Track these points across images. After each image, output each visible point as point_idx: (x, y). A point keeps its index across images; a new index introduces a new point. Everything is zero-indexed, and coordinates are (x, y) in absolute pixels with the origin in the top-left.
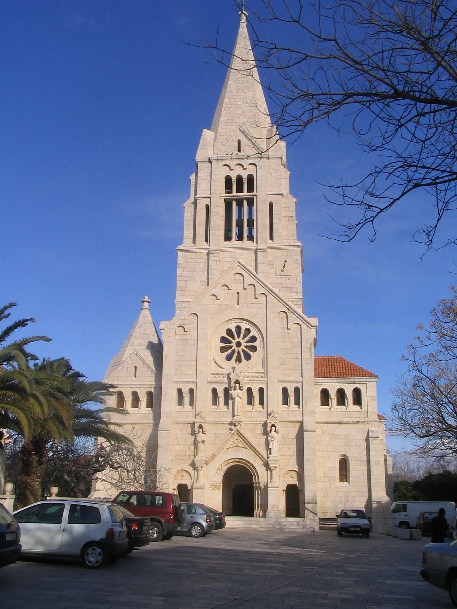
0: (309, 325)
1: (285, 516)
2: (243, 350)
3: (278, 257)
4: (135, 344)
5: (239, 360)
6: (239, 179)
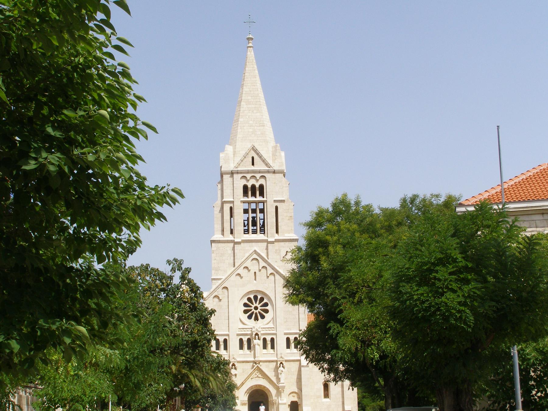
2: (259, 312)
5: (256, 319)
6: (253, 187)
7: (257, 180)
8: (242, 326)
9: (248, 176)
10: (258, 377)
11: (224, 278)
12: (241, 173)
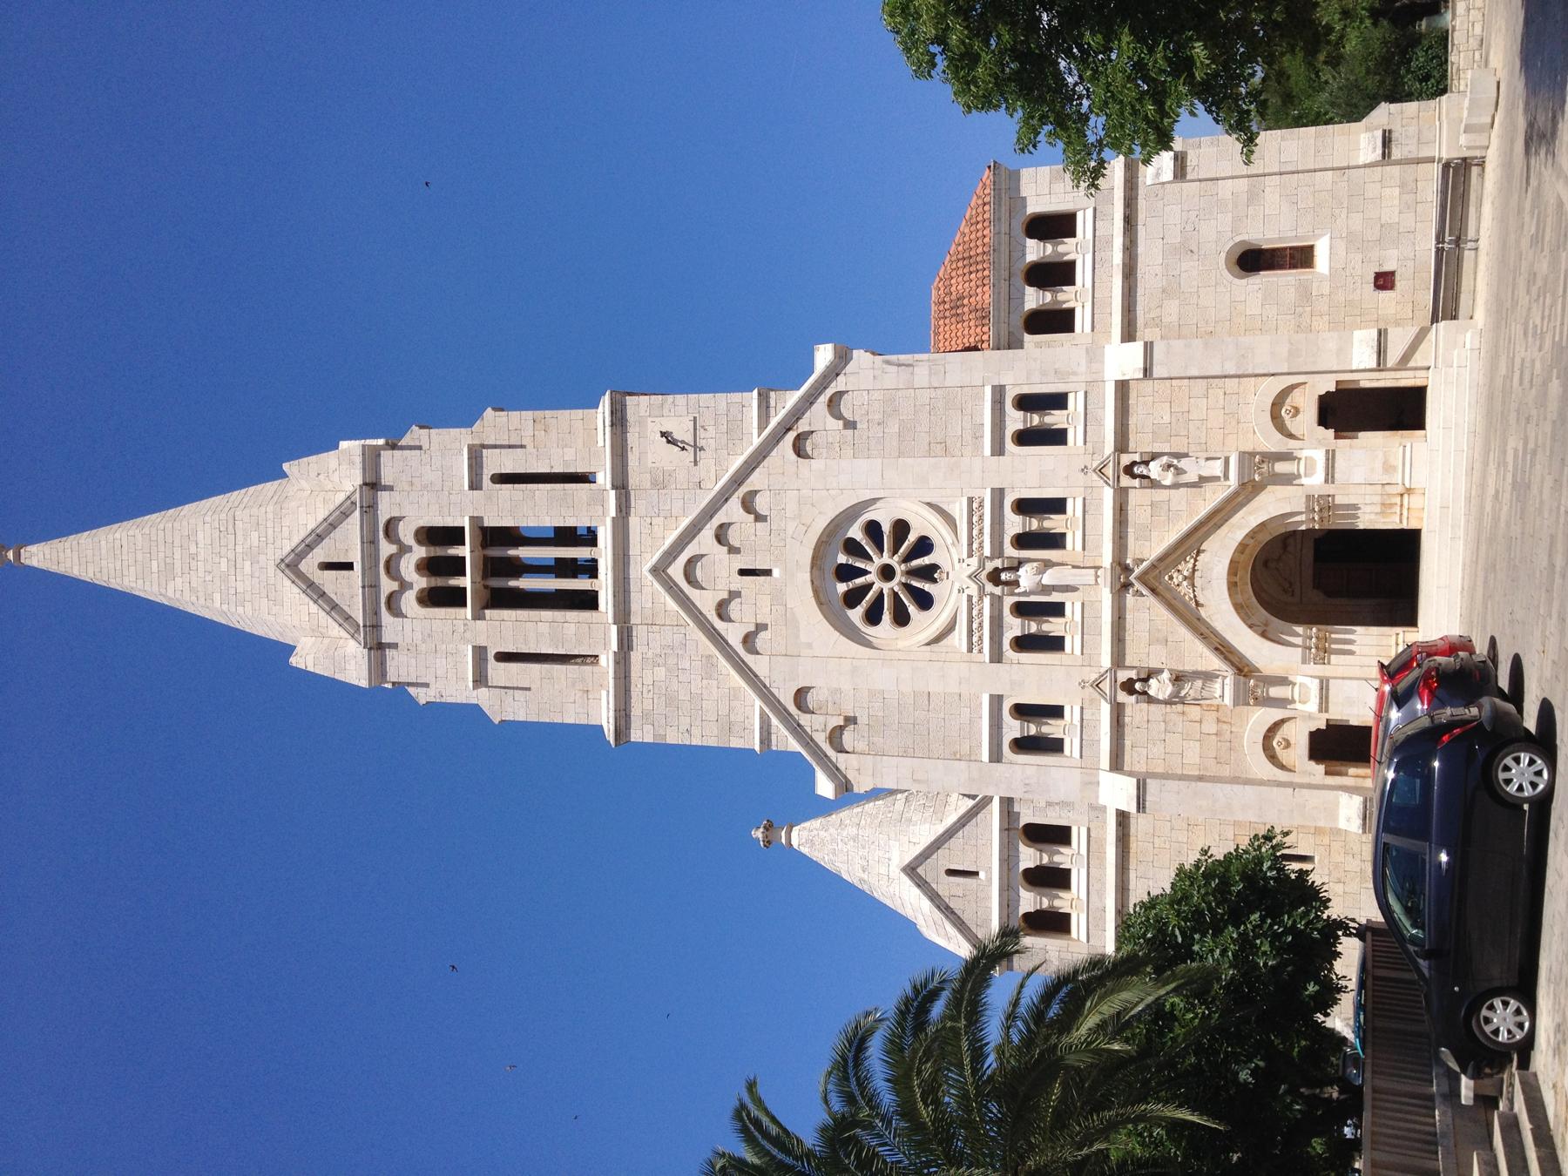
0: (833, 372)
1: (1421, 432)
3: (660, 464)
4: (883, 870)
5: (929, 573)
7: (404, 549)
8: (959, 638)
9: (387, 586)
10: (1191, 579)
11: (758, 703)
12: (377, 613)
